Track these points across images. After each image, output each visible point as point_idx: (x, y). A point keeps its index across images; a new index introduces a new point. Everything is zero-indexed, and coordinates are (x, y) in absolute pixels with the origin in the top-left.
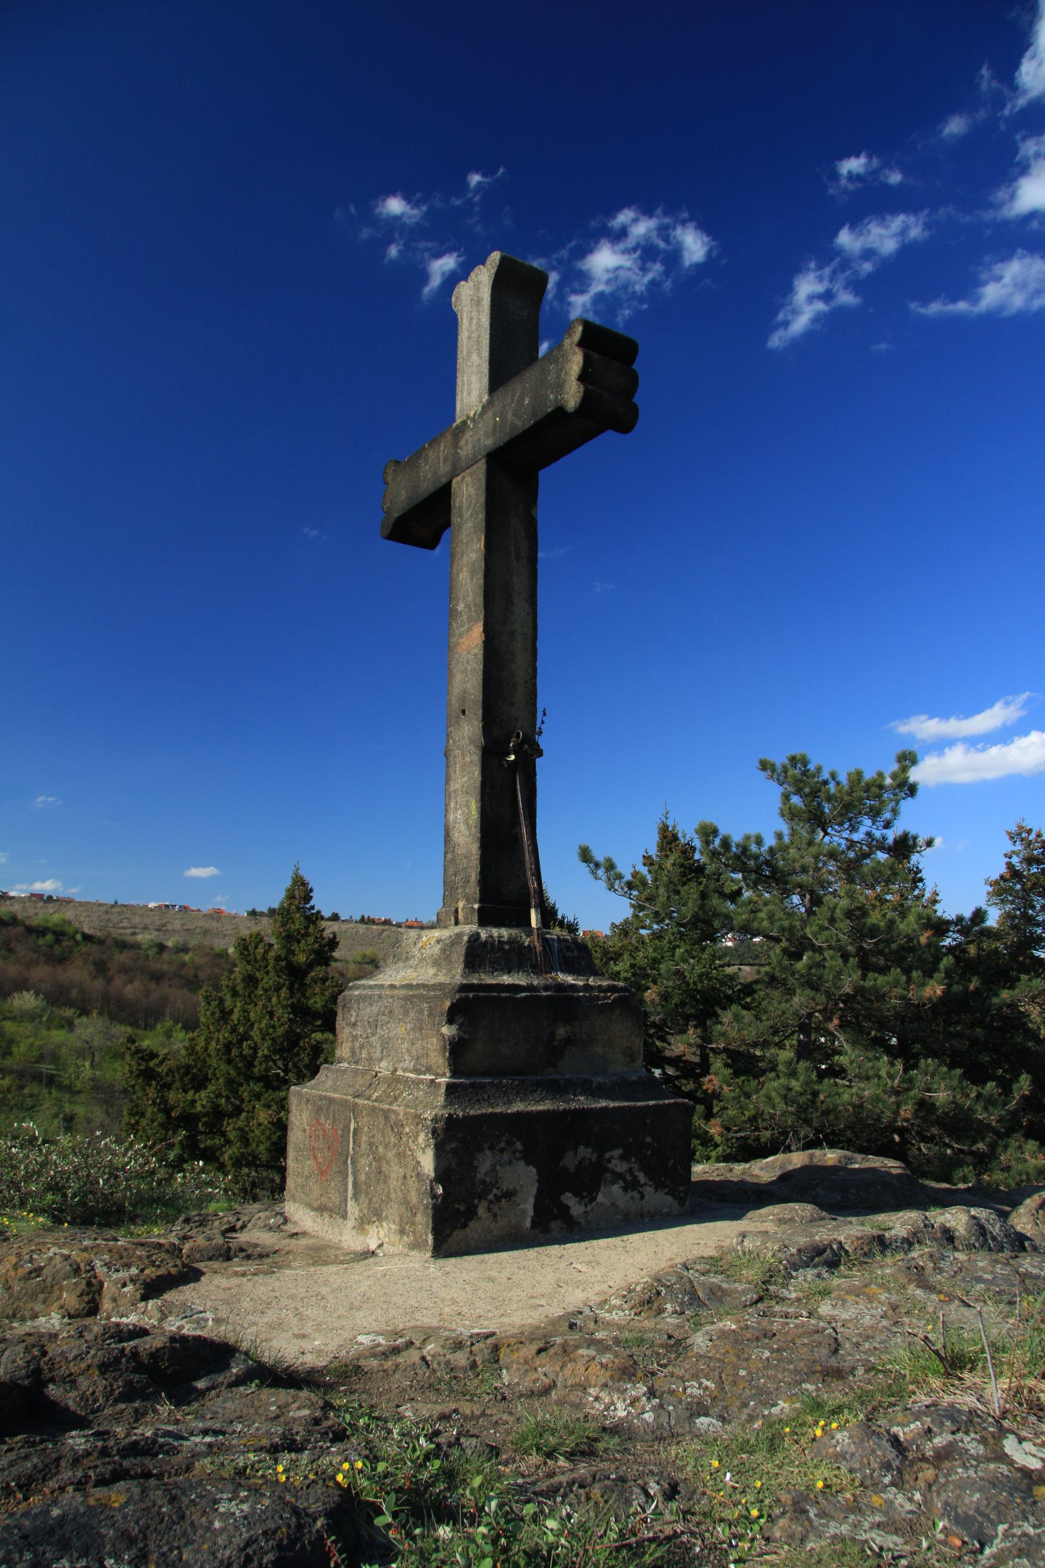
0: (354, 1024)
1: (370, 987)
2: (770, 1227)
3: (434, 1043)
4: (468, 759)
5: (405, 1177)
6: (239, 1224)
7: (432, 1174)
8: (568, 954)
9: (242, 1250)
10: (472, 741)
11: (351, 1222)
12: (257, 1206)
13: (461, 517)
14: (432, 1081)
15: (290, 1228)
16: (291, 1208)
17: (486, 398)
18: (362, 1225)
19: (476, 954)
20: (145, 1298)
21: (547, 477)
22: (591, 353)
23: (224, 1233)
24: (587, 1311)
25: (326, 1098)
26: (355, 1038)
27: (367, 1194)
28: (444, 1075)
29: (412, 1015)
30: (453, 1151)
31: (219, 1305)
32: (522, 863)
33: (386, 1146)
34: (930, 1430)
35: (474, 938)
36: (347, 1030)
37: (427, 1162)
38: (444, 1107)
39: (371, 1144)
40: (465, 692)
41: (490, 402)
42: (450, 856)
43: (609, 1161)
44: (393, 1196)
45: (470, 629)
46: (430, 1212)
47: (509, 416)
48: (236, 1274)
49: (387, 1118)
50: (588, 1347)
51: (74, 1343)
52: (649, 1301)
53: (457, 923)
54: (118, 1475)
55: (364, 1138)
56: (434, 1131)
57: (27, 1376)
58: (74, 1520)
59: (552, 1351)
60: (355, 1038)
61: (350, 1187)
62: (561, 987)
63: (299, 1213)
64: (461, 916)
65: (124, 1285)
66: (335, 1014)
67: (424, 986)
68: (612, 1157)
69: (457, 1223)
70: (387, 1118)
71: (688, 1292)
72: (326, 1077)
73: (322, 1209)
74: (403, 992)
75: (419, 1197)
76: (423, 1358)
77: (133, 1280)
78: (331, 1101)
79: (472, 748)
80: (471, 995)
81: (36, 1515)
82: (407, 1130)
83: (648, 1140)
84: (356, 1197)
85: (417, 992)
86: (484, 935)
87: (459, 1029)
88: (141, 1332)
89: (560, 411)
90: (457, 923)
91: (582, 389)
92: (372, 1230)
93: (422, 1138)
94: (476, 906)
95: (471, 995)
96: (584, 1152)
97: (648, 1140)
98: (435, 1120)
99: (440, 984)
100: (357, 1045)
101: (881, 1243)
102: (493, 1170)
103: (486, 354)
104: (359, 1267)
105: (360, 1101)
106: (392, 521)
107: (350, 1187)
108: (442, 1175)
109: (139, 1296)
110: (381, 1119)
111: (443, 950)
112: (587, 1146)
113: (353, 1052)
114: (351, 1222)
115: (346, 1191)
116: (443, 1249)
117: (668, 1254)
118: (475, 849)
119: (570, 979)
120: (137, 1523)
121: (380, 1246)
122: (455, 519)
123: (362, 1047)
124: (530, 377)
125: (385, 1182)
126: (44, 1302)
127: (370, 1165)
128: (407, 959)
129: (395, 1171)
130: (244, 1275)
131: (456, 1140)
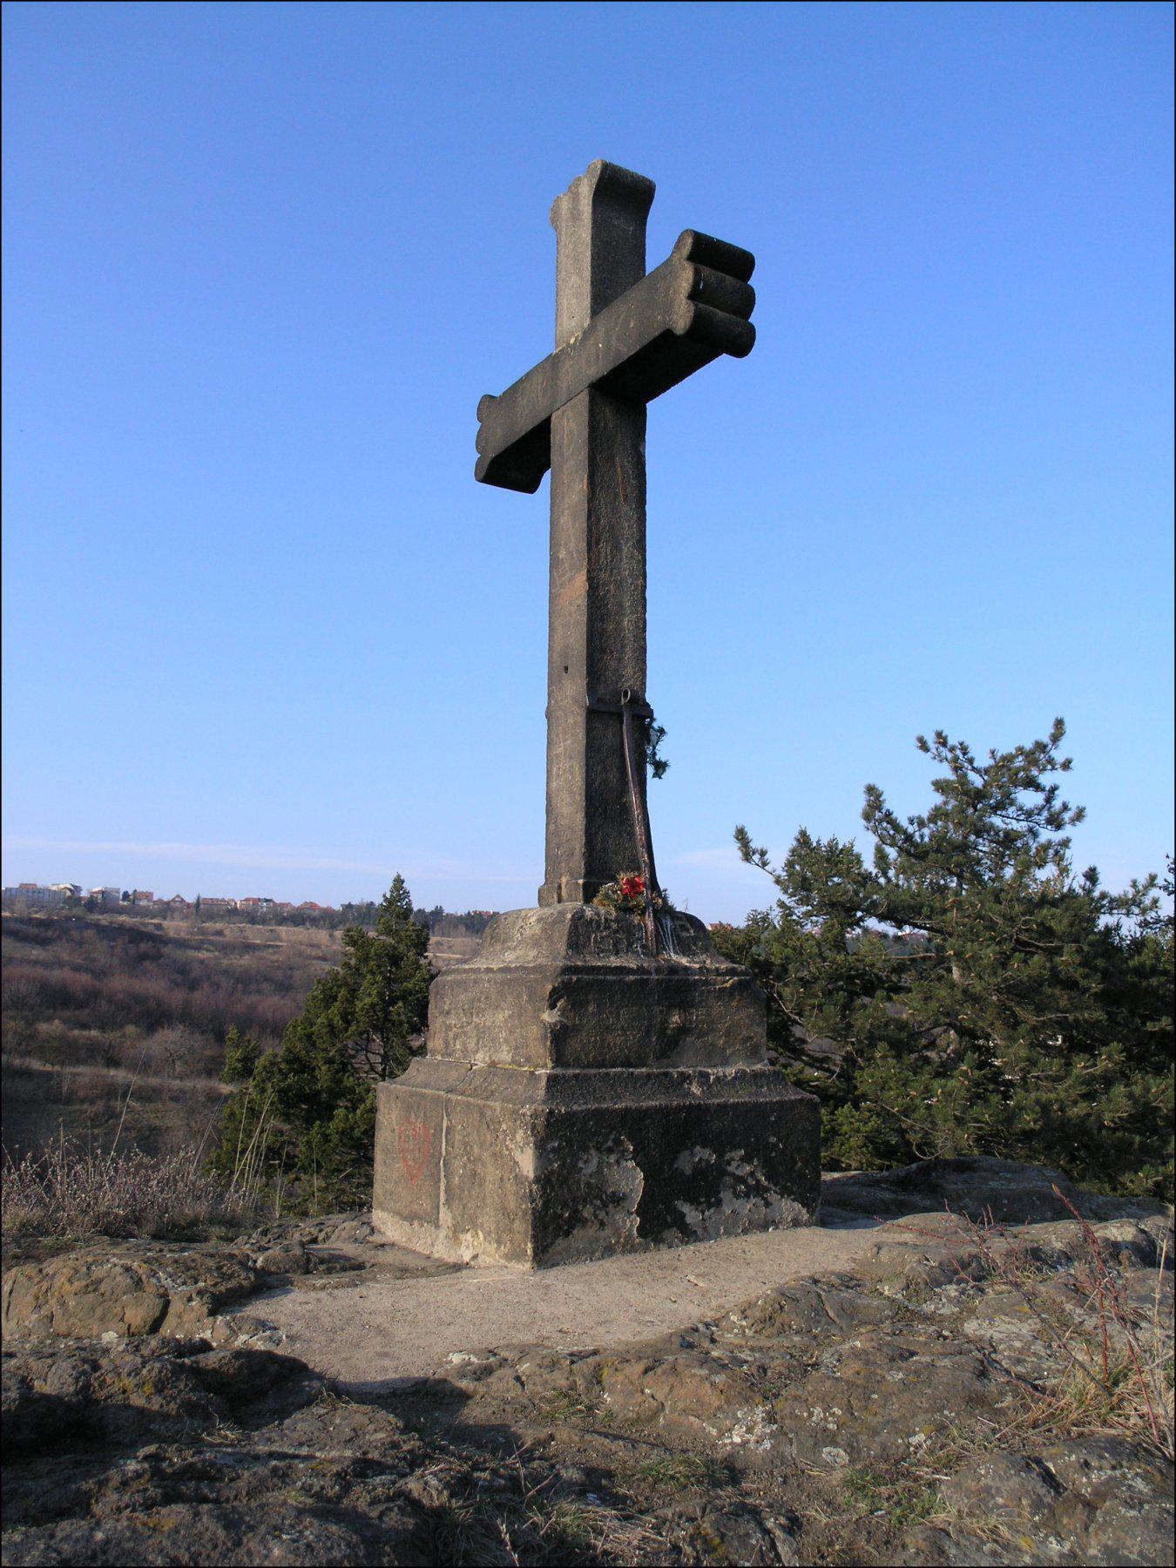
0: (448, 1013)
1: (466, 971)
2: (908, 1237)
3: (535, 1031)
4: (571, 721)
5: (502, 1179)
6: (321, 1236)
7: (531, 1175)
8: (684, 934)
9: (322, 1261)
10: (576, 701)
11: (443, 1233)
12: (342, 1216)
13: (562, 454)
14: (532, 1073)
15: (376, 1239)
16: (378, 1216)
17: (588, 321)
18: (456, 1231)
19: (579, 933)
20: (213, 1313)
21: (656, 409)
22: (702, 267)
23: (302, 1244)
24: (701, 1327)
25: (417, 1094)
26: (449, 1028)
27: (461, 1199)
28: (545, 1066)
29: (510, 999)
30: (554, 1150)
31: (300, 1321)
32: (632, 834)
33: (481, 1146)
34: (1086, 1464)
35: (578, 917)
36: (440, 1020)
37: (527, 1163)
38: (544, 1102)
39: (466, 1144)
40: (567, 647)
41: (592, 327)
42: (552, 827)
43: (729, 1163)
44: (489, 1201)
45: (572, 578)
46: (529, 1217)
47: (614, 342)
48: (314, 1288)
49: (482, 1115)
50: (701, 1366)
51: (129, 1358)
52: (770, 1318)
53: (560, 901)
54: (169, 1498)
55: (457, 1137)
56: (534, 1128)
57: (77, 1393)
58: (119, 1544)
59: (659, 1370)
60: (449, 1028)
61: (442, 1193)
62: (674, 969)
63: (387, 1224)
64: (564, 893)
65: (190, 1299)
66: (428, 1003)
67: (523, 968)
68: (732, 1159)
69: (558, 1223)
70: (482, 1115)
71: (815, 1306)
72: (417, 1070)
73: (411, 1218)
74: (499, 976)
75: (520, 1207)
76: (518, 1379)
77: (200, 1293)
78: (423, 1097)
79: (576, 708)
80: (575, 978)
81: (77, 1540)
82: (504, 1126)
83: (773, 1139)
84: (448, 1202)
85: (514, 975)
86: (589, 912)
87: (562, 1015)
88: (205, 1347)
89: (668, 334)
90: (560, 901)
91: (692, 308)
92: (467, 1237)
93: (520, 1134)
94: (581, 881)
95: (575, 978)
96: (704, 1154)
97: (773, 1139)
98: (535, 1115)
99: (540, 966)
100: (451, 1035)
101: (1036, 1255)
102: (599, 1171)
103: (587, 274)
104: (447, 1279)
105: (453, 1097)
106: (488, 462)
107: (442, 1193)
108: (545, 1180)
109: (205, 1310)
110: (477, 1116)
111: (544, 930)
112: (704, 1146)
113: (447, 1043)
114: (443, 1233)
115: (438, 1196)
116: (544, 1257)
117: (794, 1267)
118: (579, 820)
119: (684, 961)
120: (188, 1549)
121: (475, 1257)
122: (554, 458)
123: (456, 1037)
124: (634, 297)
125: (480, 1185)
126: (102, 1319)
127: (465, 1167)
128: (505, 941)
129: (491, 1173)
130: (323, 1288)
131: (562, 1137)
